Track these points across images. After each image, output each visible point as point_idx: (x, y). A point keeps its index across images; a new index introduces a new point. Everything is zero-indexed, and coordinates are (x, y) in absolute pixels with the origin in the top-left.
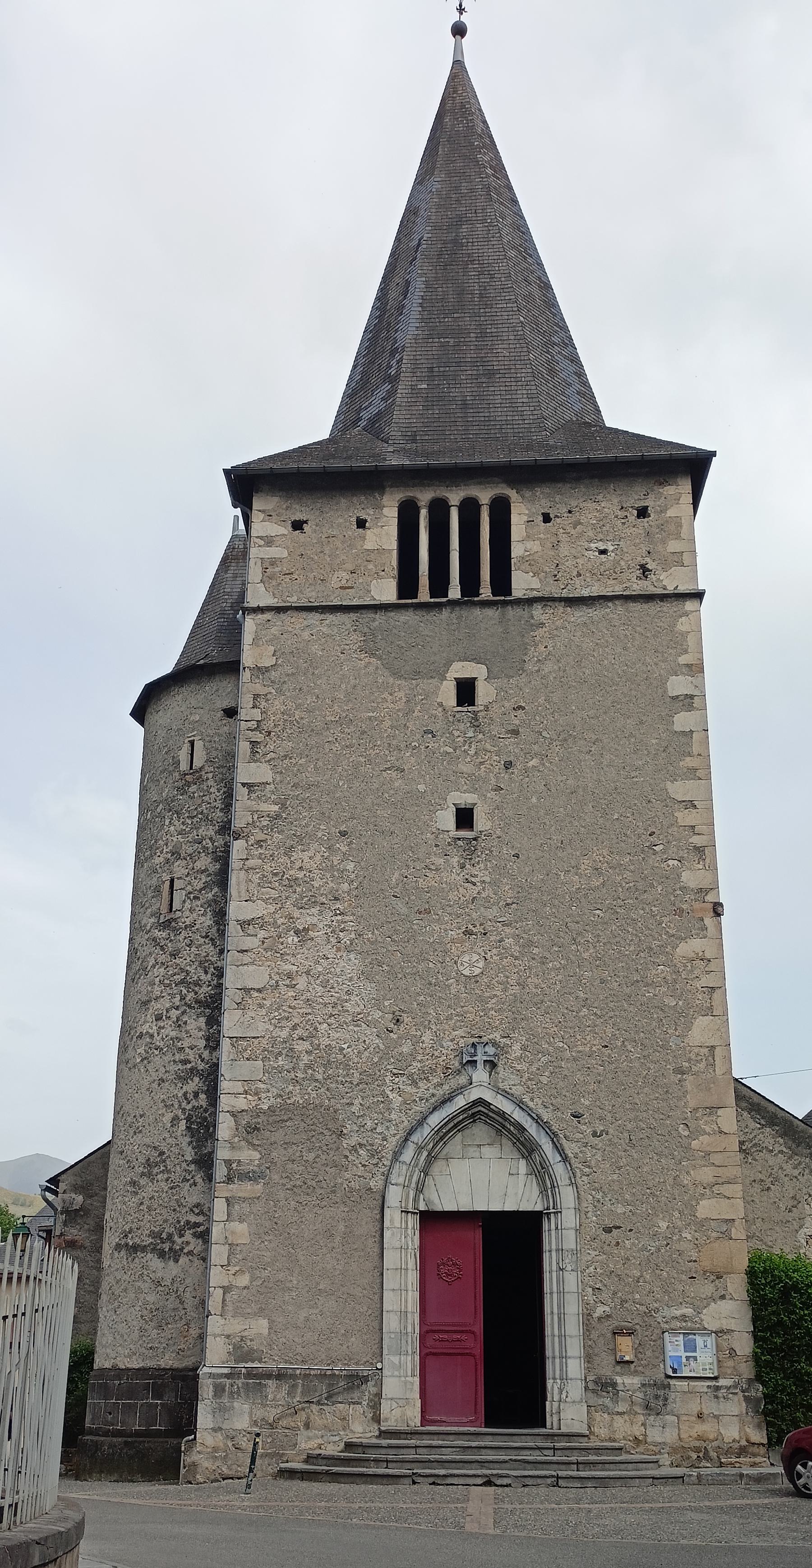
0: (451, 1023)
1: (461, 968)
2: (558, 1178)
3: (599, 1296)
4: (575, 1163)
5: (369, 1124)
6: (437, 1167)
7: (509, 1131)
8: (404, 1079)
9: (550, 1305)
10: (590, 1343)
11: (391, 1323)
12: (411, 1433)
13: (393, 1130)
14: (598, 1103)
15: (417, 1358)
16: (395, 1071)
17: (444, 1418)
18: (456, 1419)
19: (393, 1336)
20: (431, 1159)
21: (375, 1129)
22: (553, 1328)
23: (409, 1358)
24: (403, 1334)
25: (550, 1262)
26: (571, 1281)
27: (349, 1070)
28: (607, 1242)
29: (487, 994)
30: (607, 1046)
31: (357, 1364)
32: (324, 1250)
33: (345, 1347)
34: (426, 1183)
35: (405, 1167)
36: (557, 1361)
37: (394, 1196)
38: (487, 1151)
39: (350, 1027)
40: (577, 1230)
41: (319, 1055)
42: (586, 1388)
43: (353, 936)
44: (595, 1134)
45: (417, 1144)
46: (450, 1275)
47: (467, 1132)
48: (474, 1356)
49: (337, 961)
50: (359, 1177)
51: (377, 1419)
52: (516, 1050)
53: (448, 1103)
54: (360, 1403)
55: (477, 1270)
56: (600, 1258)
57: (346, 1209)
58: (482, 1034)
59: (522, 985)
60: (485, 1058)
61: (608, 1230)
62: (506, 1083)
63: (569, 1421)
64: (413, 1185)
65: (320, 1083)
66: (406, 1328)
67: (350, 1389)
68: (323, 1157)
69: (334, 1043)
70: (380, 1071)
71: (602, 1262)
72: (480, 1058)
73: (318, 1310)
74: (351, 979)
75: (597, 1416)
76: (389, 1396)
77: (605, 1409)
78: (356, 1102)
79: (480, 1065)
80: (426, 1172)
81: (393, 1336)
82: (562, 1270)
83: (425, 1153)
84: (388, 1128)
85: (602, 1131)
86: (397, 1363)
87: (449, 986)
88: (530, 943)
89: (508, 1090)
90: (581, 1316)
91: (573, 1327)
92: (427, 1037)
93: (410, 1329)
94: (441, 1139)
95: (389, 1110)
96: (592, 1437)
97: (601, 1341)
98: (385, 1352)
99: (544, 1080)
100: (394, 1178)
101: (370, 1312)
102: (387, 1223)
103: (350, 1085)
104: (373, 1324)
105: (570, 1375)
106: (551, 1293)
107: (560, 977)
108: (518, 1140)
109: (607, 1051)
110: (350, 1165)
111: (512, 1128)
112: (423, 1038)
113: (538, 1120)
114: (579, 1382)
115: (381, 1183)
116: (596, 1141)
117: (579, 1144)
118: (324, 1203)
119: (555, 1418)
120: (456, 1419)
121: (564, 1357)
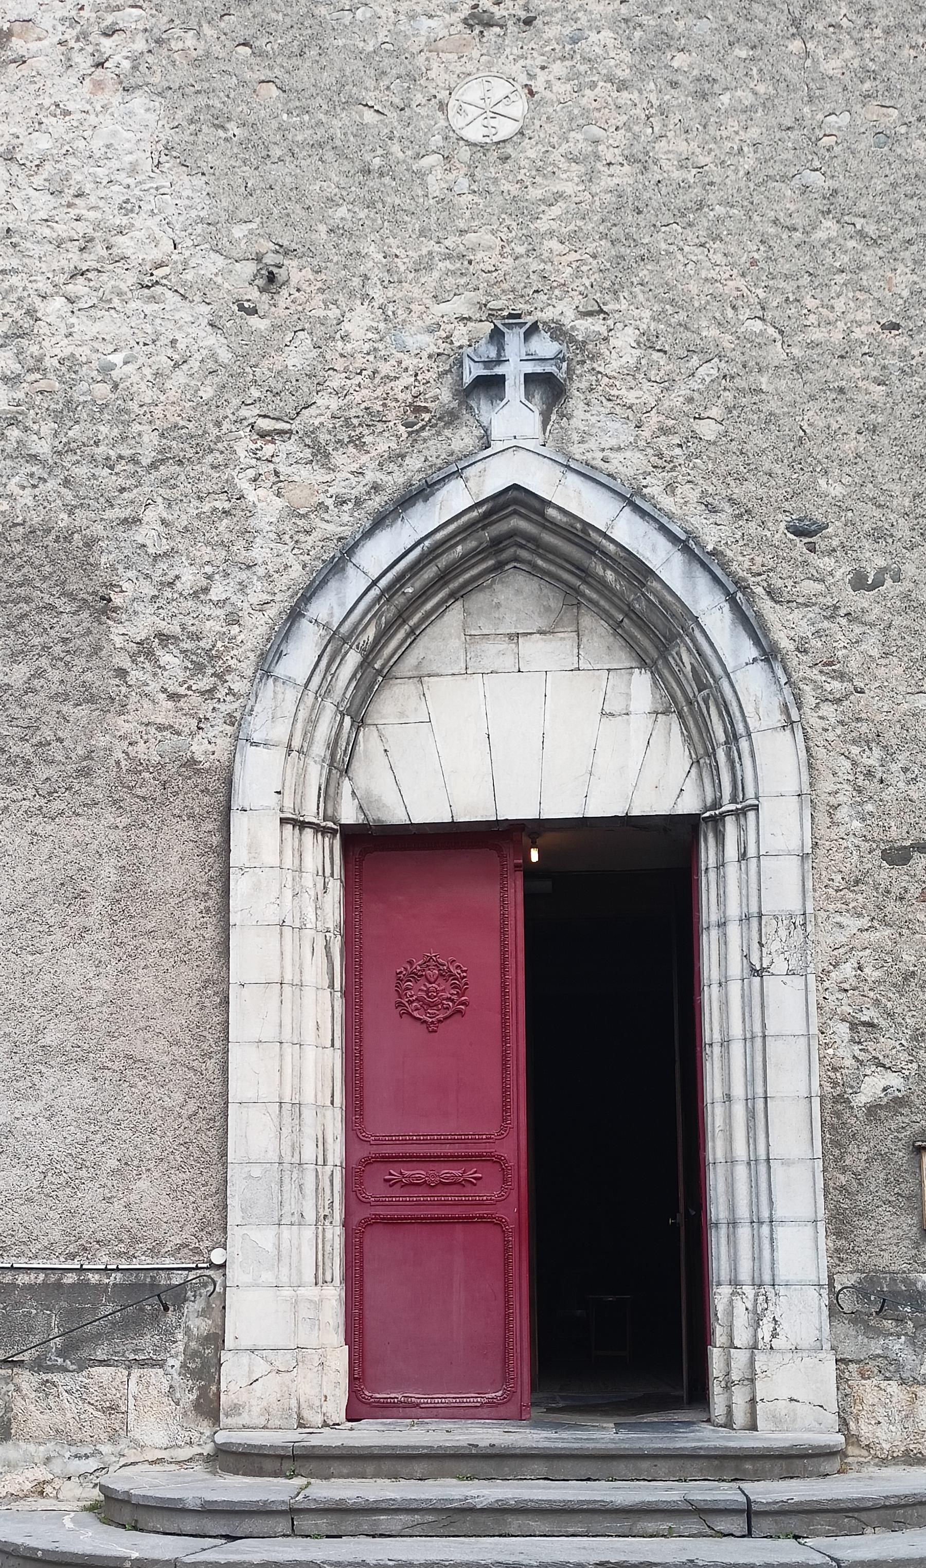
0: (430, 279)
1: (457, 122)
2: (749, 710)
3: (870, 1046)
4: (801, 667)
5: (189, 578)
6: (393, 703)
7: (602, 586)
8: (291, 446)
9: (723, 1079)
10: (843, 1179)
11: (252, 1135)
12: (294, 1457)
13: (256, 596)
14: (870, 490)
15: (335, 1234)
16: (265, 424)
17: (415, 1396)
18: (449, 1398)
19: (257, 1171)
20: (373, 678)
21: (206, 590)
22: (730, 1140)
23: (309, 1233)
24: (288, 1167)
25: (720, 958)
26: (788, 1004)
27: (128, 424)
28: (896, 890)
29: (535, 193)
30: (896, 326)
31: (154, 1252)
32: (59, 937)
33: (118, 1206)
34: (360, 748)
35: (291, 695)
36: (744, 1233)
37: (264, 781)
38: (537, 651)
39: (133, 305)
40: (804, 857)
41: (43, 385)
42: (834, 1310)
43: (140, 45)
44: (859, 582)
45: (326, 626)
46: (430, 1005)
47: (479, 600)
48: (499, 1223)
49: (92, 119)
50: (160, 728)
51: (209, 1407)
52: (623, 348)
53: (420, 506)
54: (161, 1364)
55: (511, 990)
56: (873, 936)
57: (124, 821)
58: (521, 307)
59: (641, 162)
60: (530, 368)
61: (897, 856)
62: (592, 444)
63: (783, 1407)
64: (319, 749)
65: (43, 463)
66: (296, 1148)
67: (131, 1325)
68: (55, 675)
69: (86, 350)
70: (218, 424)
71: (878, 948)
72: (514, 370)
73: (40, 1105)
74: (133, 170)
75: (869, 1391)
76: (246, 1343)
77: (891, 1368)
78: (150, 515)
79: (514, 389)
80: (358, 713)
81: (257, 1171)
82: (759, 973)
83: (353, 659)
84: (243, 587)
85: (882, 571)
86: (270, 1246)
87: (421, 175)
88: (664, 41)
89: (599, 463)
90: (816, 1102)
91: (794, 1135)
92: (359, 323)
93: (309, 1153)
94: (401, 617)
95: (247, 535)
96: (851, 1450)
97: (878, 1173)
98: (234, 1217)
99: (708, 430)
100: (258, 727)
101: (192, 1106)
102: (235, 859)
103: (131, 467)
104: (202, 1139)
105: (783, 1275)
106: (726, 1043)
107: (754, 133)
108: (630, 612)
109: (896, 341)
110: (134, 698)
111: (610, 576)
112: (346, 326)
113: (686, 545)
114: (812, 1292)
115: (223, 745)
116: (863, 600)
117: (812, 613)
118: (57, 805)
119: (740, 1397)
120: (449, 1398)
121: (764, 1222)
